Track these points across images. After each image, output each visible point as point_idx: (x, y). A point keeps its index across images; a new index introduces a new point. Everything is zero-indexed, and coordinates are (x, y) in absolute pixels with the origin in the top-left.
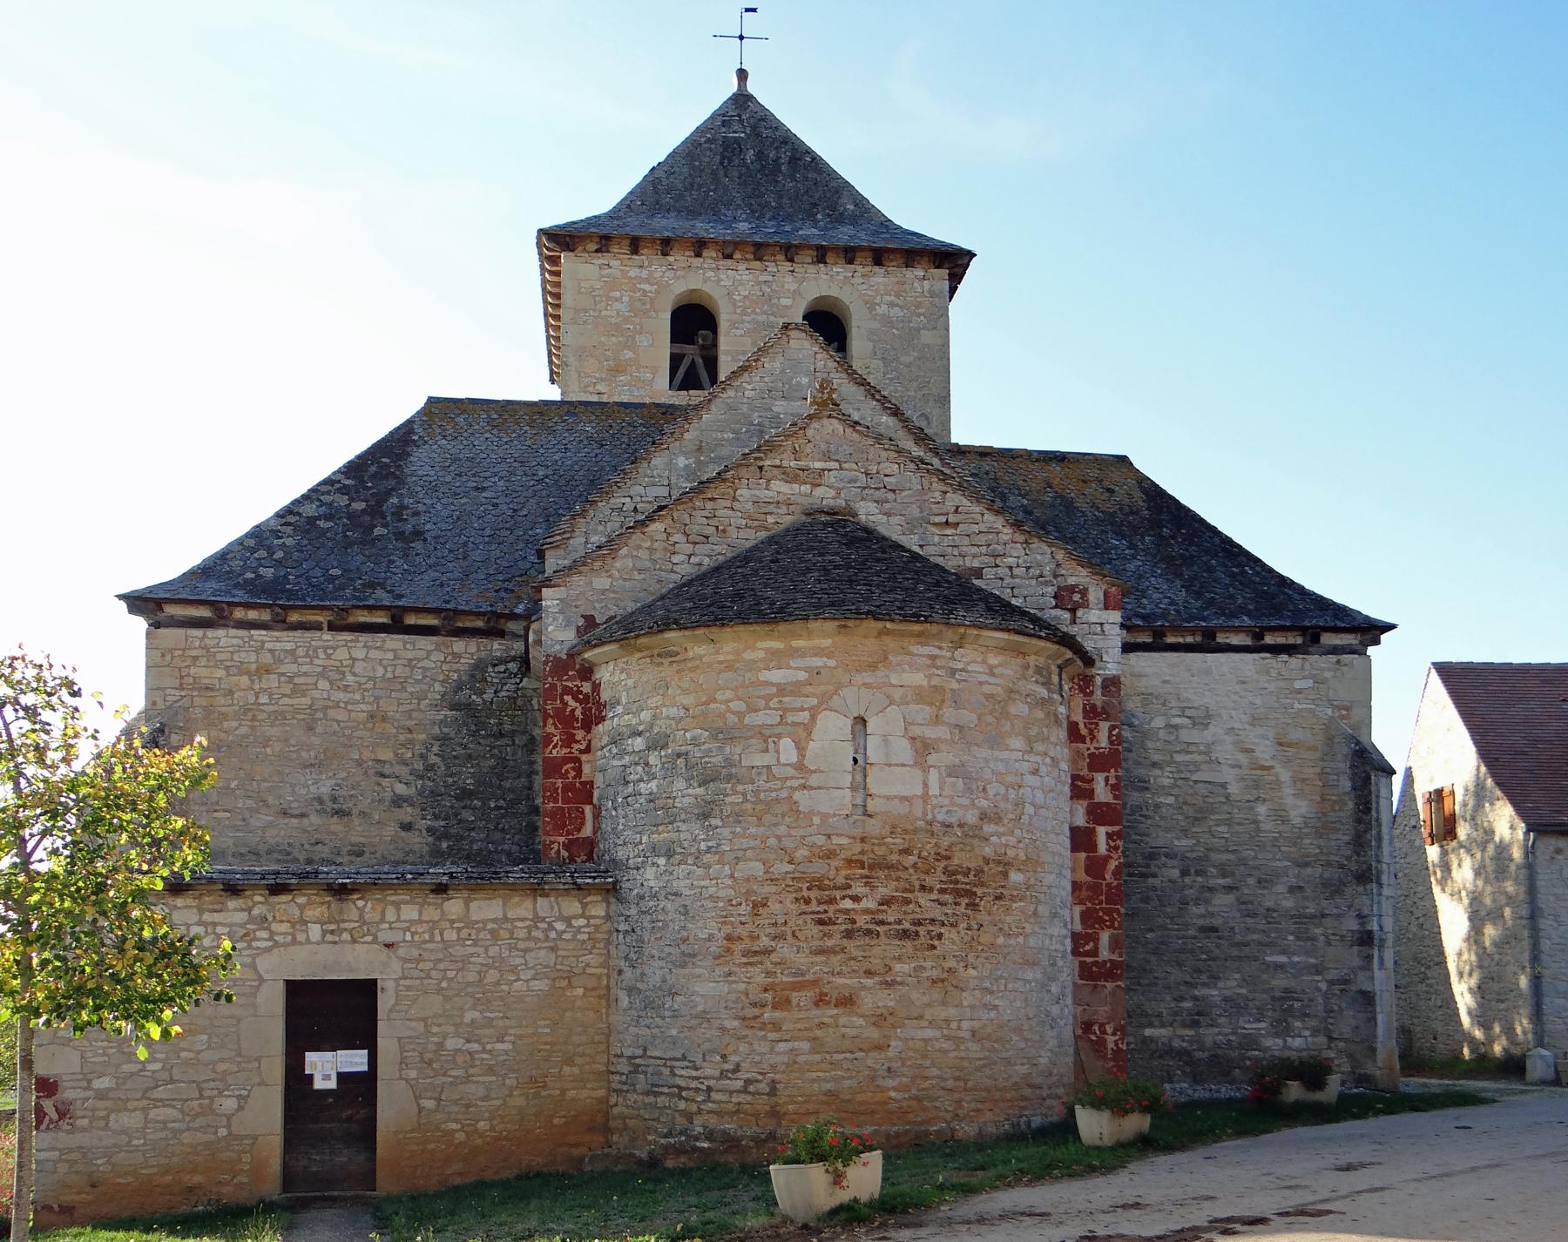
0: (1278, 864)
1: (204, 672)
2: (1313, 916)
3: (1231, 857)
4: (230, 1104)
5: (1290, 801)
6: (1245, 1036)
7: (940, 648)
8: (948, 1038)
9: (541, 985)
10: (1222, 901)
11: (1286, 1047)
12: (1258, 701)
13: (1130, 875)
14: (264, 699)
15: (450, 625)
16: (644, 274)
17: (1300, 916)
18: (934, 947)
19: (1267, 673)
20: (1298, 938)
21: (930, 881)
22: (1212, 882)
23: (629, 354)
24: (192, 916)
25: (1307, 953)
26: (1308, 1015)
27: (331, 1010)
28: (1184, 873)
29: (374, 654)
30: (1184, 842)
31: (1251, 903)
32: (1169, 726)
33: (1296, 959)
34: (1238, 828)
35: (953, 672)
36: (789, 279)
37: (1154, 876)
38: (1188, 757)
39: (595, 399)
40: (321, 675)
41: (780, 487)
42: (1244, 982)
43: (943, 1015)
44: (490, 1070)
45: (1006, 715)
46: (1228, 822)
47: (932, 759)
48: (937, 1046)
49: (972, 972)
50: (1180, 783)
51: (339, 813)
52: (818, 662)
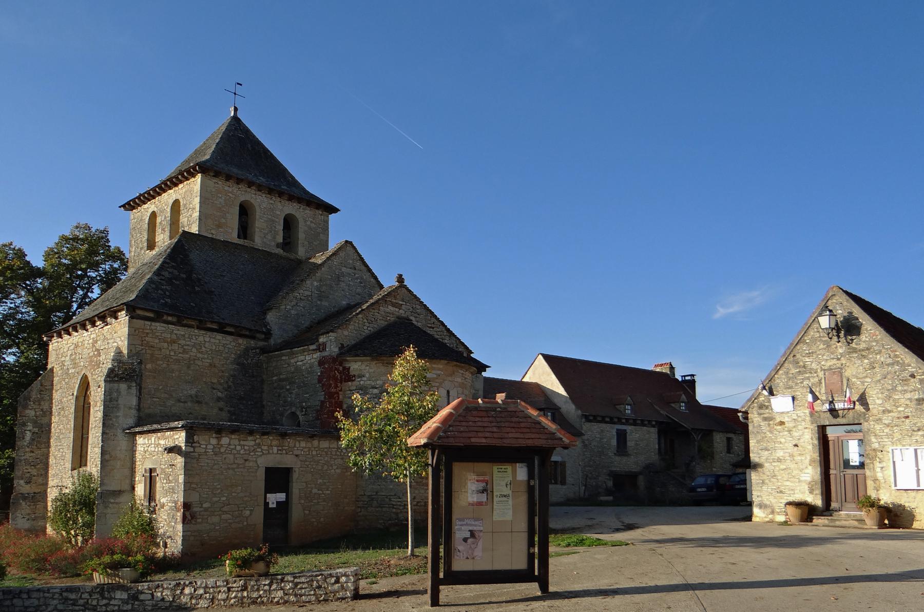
1: (150, 339)
4: (248, 513)
9: (338, 471)
14: (172, 353)
15: (238, 333)
16: (230, 190)
23: (223, 221)
24: (237, 442)
27: (278, 479)
29: (212, 340)
39: (210, 236)
40: (194, 346)
41: (391, 308)
44: (324, 501)
51: (199, 402)
52: (439, 372)
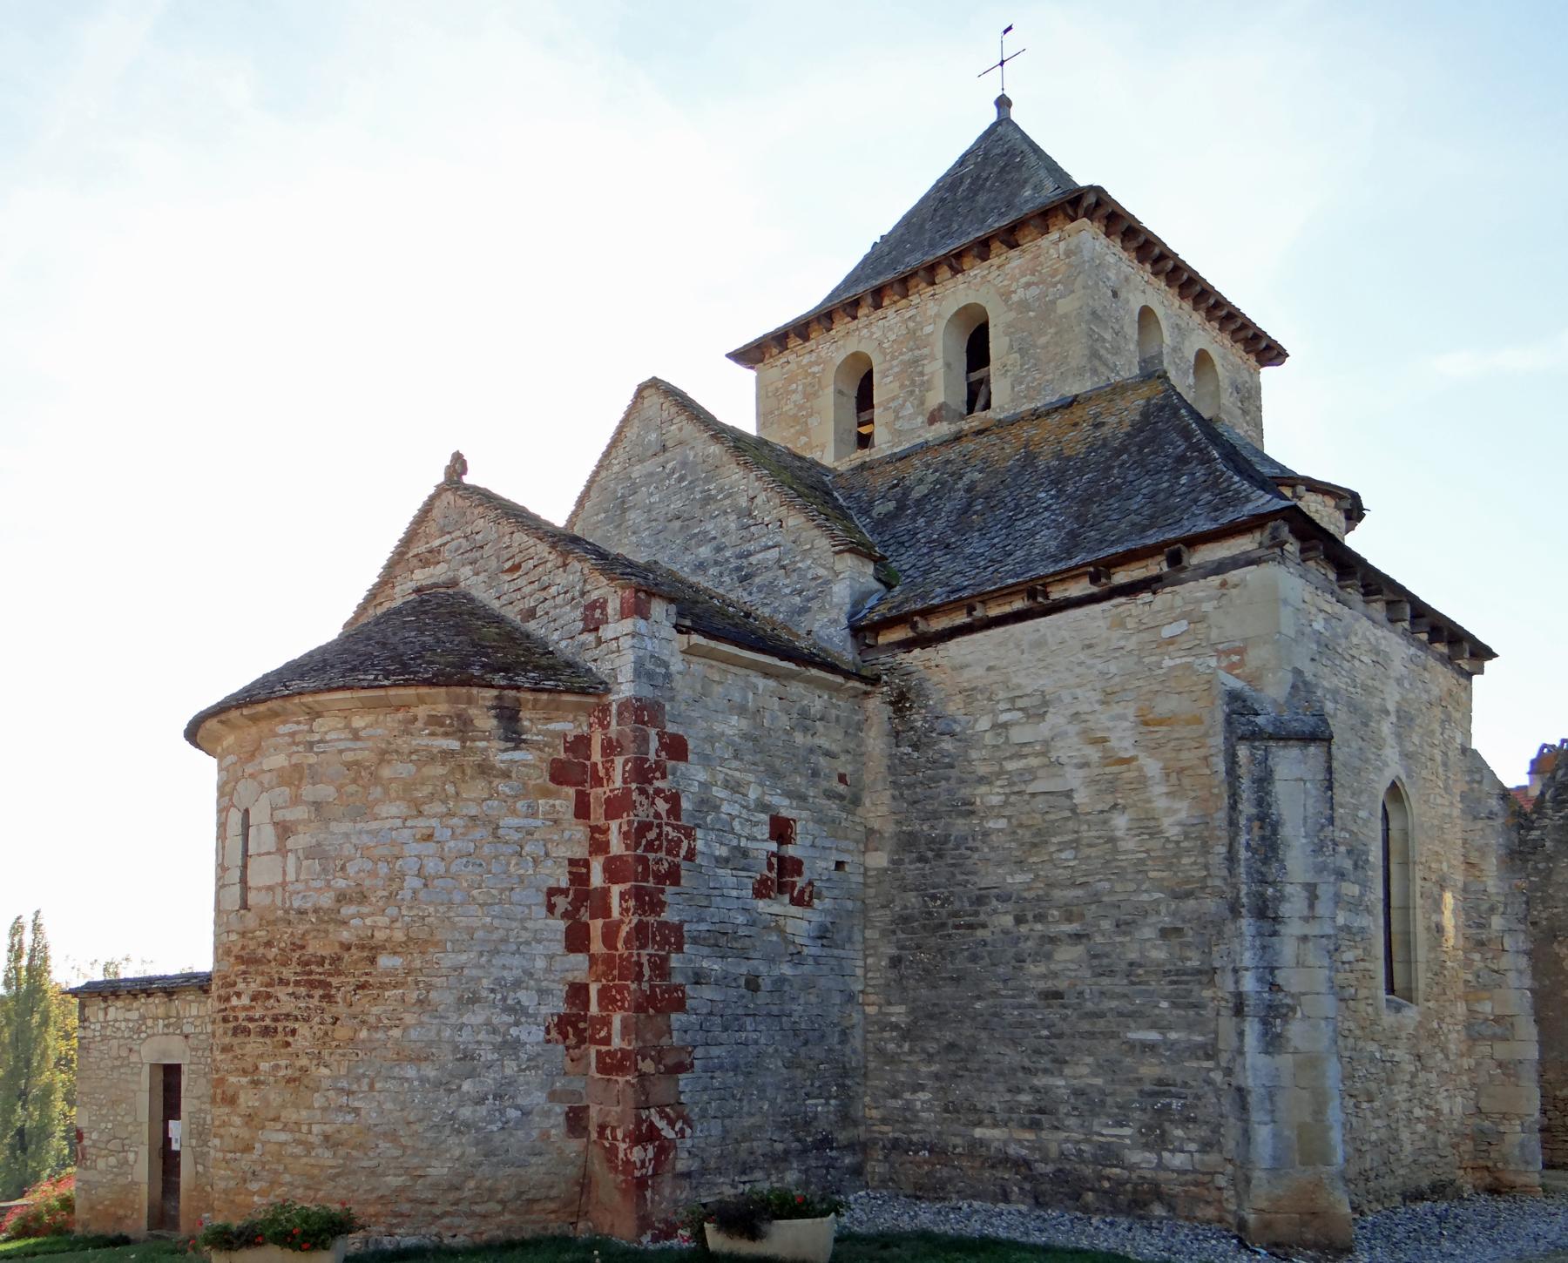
0: (1145, 897)
2: (1199, 972)
3: (1080, 892)
5: (1161, 803)
6: (1101, 1146)
7: (298, 723)
8: (299, 1142)
10: (1067, 955)
11: (1161, 1166)
12: (1113, 669)
13: (958, 927)
17: (1178, 973)
18: (288, 1044)
19: (1122, 625)
20: (1174, 1005)
21: (287, 973)
22: (1053, 930)
25: (1190, 1027)
26: (1194, 1120)
28: (1019, 920)
30: (1019, 878)
31: (1107, 955)
32: (995, 726)
33: (1173, 1036)
34: (1088, 851)
35: (311, 745)
36: (931, 304)
37: (984, 926)
38: (1021, 764)
42: (1099, 1069)
43: (294, 1117)
45: (375, 779)
46: (1075, 844)
47: (290, 844)
48: (290, 1150)
49: (324, 1071)
50: (1013, 799)
